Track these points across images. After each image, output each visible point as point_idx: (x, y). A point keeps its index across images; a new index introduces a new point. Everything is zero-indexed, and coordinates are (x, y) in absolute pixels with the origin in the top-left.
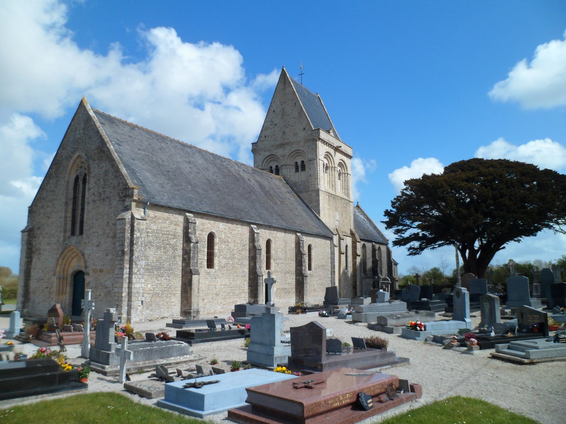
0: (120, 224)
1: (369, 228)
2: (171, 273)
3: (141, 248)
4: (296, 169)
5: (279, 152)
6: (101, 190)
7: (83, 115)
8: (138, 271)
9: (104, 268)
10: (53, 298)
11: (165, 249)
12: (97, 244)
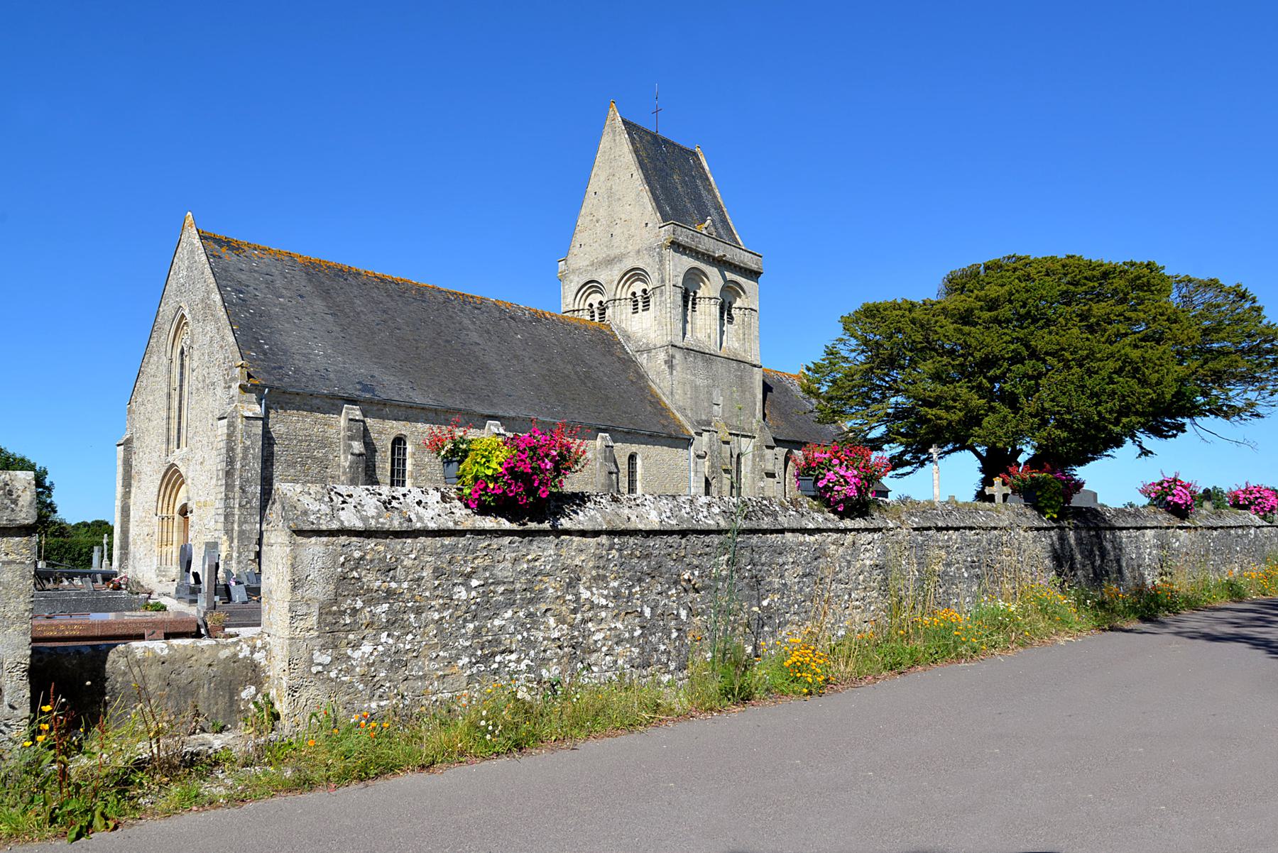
4: (634, 305)
5: (602, 276)
8: (247, 503)
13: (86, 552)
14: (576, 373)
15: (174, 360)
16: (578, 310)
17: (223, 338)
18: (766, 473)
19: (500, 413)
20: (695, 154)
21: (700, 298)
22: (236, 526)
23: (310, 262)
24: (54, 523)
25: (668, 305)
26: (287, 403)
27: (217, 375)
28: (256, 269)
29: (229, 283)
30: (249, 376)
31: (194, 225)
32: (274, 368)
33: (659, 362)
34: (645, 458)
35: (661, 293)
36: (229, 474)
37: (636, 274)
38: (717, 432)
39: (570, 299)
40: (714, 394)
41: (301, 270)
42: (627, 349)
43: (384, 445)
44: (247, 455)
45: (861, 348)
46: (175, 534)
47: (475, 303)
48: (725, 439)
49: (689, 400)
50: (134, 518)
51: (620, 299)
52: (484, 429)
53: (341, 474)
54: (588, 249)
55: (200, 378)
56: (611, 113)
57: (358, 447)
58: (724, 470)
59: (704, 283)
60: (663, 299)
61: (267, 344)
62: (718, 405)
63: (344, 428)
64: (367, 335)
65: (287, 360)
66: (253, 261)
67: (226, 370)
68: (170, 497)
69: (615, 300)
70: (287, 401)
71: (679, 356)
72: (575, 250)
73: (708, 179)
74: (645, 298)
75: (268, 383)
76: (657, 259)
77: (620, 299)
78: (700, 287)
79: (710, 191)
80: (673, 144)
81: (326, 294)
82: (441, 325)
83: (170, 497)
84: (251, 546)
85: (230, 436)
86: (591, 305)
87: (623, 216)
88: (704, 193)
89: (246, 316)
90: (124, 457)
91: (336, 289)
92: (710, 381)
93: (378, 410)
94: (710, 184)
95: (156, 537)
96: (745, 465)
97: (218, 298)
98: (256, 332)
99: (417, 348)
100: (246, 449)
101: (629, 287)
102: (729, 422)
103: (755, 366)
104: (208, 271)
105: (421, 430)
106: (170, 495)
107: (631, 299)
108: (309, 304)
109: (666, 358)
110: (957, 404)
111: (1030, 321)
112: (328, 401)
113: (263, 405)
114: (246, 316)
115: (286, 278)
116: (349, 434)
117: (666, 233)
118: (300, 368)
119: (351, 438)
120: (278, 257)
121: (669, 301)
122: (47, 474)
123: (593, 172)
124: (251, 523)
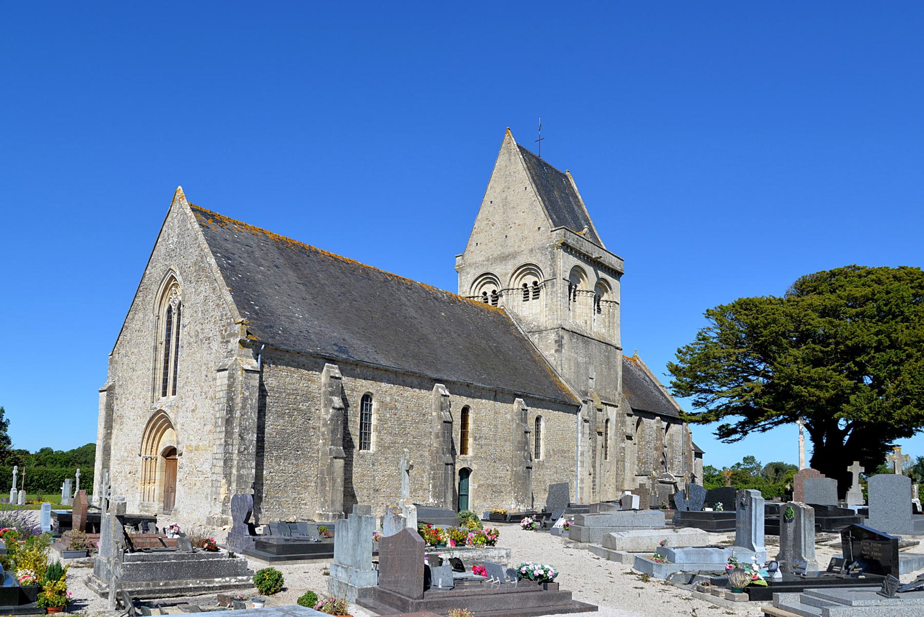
0: (220, 378)
1: (652, 393)
2: (299, 455)
3: (251, 415)
5: (497, 270)
6: (198, 328)
7: (178, 214)
8: (245, 449)
9: (201, 444)
10: (137, 488)
11: (290, 416)
12: (193, 408)
13: (37, 479)
14: (490, 347)
15: (161, 317)
16: (474, 297)
17: (219, 297)
18: (627, 436)
19: (445, 378)
20: (566, 177)
21: (580, 291)
22: (234, 471)
23: (279, 239)
24: (9, 453)
25: (559, 295)
26: (278, 359)
27: (212, 330)
28: (238, 240)
29: (219, 250)
30: (248, 333)
31: (184, 198)
32: (266, 327)
33: (550, 341)
34: (548, 421)
35: (553, 285)
36: (228, 422)
37: (529, 269)
38: (592, 401)
39: (466, 288)
40: (590, 370)
41: (273, 245)
42: (520, 330)
43: (355, 400)
44: (246, 405)
45: (919, 328)
46: (158, 474)
47: (406, 284)
48: (599, 408)
49: (573, 374)
50: (115, 456)
51: (513, 289)
52: (432, 390)
53: (321, 425)
54: (483, 247)
55: (192, 333)
56: (507, 137)
57: (337, 402)
58: (598, 433)
59: (583, 279)
60: (555, 289)
61: (257, 306)
62: (592, 379)
63: (325, 385)
64: (333, 304)
65: (275, 321)
66: (235, 234)
67: (223, 326)
68: (154, 440)
69: (509, 290)
70: (279, 357)
71: (566, 337)
72: (472, 247)
73: (577, 197)
74: (535, 289)
75: (264, 340)
76: (549, 257)
77: (513, 289)
78: (580, 282)
79: (580, 206)
80: (550, 167)
81: (295, 266)
82: (386, 300)
83: (154, 440)
84: (248, 489)
85: (230, 386)
86: (485, 293)
87: (517, 221)
88: (576, 208)
89: (236, 280)
90: (107, 402)
91: (302, 263)
92: (588, 359)
93: (351, 369)
94: (579, 201)
95: (139, 475)
96: (611, 429)
97: (213, 261)
98: (246, 294)
99: (372, 318)
100: (245, 399)
101: (521, 279)
102: (599, 392)
103: (617, 348)
104: (201, 237)
105: (384, 389)
106: (154, 438)
107: (522, 289)
108: (284, 273)
109: (557, 338)
110: (829, 384)
111: (891, 316)
112: (312, 359)
113: (259, 360)
114: (236, 280)
115: (263, 250)
116: (330, 389)
117: (557, 236)
118: (286, 328)
119: (332, 394)
120: (253, 232)
121: (559, 291)
122: (4, 412)
123: (489, 185)
124: (248, 468)
